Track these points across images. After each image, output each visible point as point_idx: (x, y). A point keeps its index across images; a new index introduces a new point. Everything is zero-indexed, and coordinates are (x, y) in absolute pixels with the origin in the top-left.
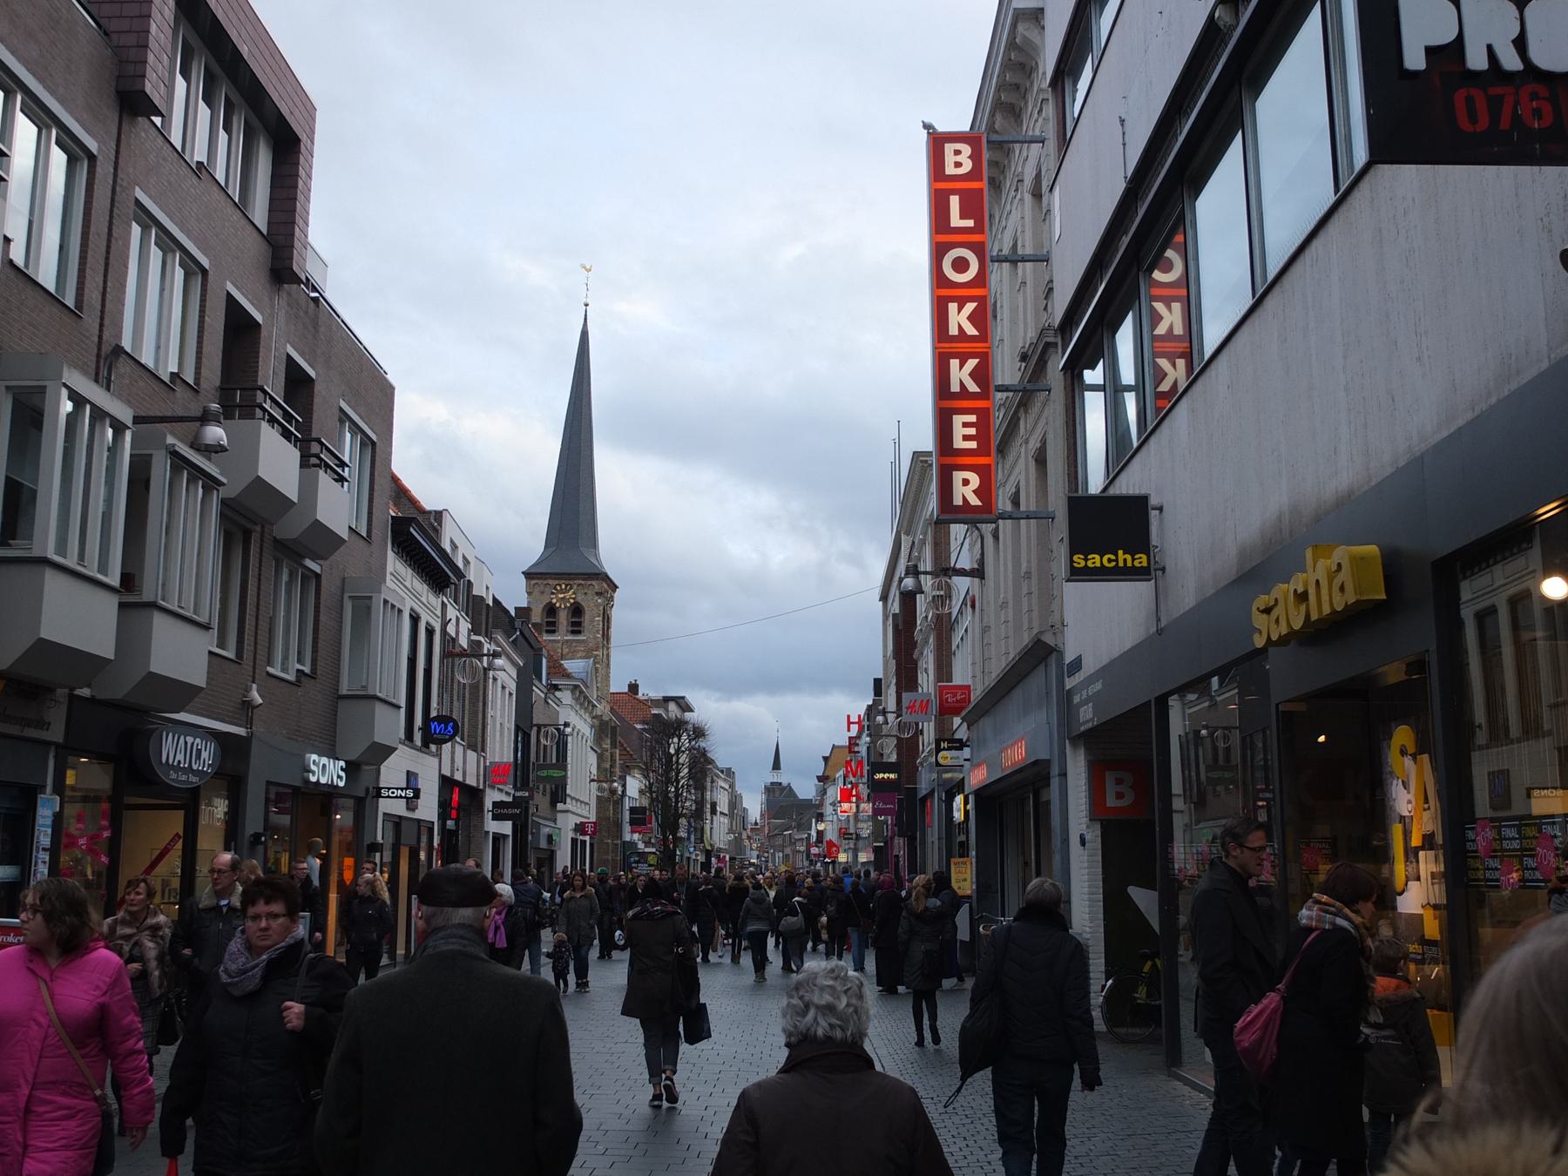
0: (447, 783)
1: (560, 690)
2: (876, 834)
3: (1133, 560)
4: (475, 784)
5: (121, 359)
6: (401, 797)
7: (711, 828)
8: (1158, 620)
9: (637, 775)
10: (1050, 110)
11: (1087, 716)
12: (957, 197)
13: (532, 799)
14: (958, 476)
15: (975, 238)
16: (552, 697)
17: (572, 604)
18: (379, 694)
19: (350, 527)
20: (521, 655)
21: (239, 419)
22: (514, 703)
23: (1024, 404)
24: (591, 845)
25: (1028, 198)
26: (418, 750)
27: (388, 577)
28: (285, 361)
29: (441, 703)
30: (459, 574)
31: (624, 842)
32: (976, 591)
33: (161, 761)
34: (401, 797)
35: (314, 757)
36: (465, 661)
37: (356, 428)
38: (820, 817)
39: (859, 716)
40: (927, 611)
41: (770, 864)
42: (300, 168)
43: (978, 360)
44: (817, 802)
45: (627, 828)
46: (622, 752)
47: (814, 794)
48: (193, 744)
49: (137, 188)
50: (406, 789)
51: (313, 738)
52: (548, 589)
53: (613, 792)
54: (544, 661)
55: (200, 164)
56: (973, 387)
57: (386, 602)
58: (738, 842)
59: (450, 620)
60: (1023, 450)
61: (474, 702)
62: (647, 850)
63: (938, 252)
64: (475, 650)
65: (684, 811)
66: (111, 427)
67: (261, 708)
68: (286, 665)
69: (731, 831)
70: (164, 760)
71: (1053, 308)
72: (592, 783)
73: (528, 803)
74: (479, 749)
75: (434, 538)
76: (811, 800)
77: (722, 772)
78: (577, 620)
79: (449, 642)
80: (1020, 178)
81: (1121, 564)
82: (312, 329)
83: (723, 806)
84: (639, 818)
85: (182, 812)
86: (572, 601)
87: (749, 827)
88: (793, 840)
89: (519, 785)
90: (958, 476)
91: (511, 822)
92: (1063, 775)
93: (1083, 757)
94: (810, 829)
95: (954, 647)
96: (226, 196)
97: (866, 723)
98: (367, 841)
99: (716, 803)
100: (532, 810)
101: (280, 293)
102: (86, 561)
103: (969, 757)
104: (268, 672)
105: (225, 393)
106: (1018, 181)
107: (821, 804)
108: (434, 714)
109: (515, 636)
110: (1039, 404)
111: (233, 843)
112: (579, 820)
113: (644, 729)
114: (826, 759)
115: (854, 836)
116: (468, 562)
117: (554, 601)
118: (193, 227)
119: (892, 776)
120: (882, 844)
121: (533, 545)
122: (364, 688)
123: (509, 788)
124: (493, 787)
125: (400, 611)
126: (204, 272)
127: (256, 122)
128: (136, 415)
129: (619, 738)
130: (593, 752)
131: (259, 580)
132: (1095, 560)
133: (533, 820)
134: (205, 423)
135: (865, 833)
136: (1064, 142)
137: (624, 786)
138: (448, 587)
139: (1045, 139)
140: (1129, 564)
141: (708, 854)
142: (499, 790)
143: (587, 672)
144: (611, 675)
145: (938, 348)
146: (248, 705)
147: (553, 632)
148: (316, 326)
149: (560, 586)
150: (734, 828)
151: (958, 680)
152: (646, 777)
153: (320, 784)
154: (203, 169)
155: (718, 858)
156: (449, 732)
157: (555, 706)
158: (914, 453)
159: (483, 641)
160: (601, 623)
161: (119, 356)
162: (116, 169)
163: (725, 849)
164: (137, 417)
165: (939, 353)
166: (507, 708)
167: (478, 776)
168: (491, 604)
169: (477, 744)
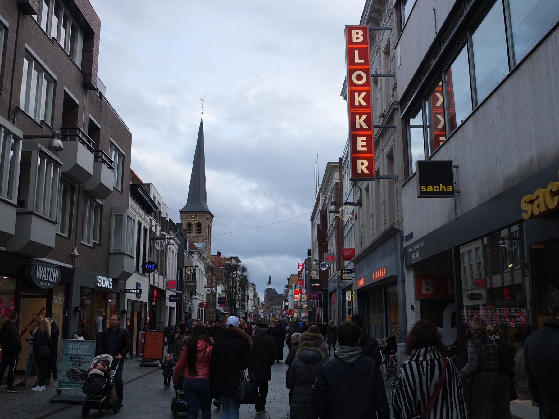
0: (152, 288)
1: (193, 254)
2: (309, 307)
3: (446, 188)
4: (162, 288)
5: (19, 112)
6: (134, 293)
7: (247, 305)
8: (456, 214)
9: (221, 285)
10: (394, 17)
11: (416, 257)
12: (358, 51)
13: (184, 294)
14: (360, 161)
15: (365, 67)
16: (190, 256)
17: (197, 223)
18: (126, 252)
19: (114, 187)
20: (179, 240)
21: (69, 141)
22: (177, 258)
23: (382, 135)
24: (205, 311)
25: (383, 55)
26: (140, 275)
27: (129, 207)
28: (88, 120)
29: (149, 257)
30: (157, 208)
31: (216, 310)
32: (357, 212)
33: (36, 278)
34: (134, 293)
35: (100, 277)
36: (159, 241)
37: (117, 149)
38: (286, 301)
39: (302, 263)
40: (333, 222)
41: (267, 318)
42: (94, 43)
43: (367, 115)
44: (284, 295)
45: (217, 305)
46: (215, 277)
47: (283, 292)
48: (50, 271)
49: (26, 44)
50: (136, 290)
51: (99, 269)
52: (188, 217)
53: (212, 291)
54: (188, 242)
55: (53, 38)
56: (365, 126)
57: (128, 216)
58: (256, 310)
59: (153, 225)
60: (381, 154)
61: (162, 257)
62: (225, 313)
63: (350, 72)
64: (163, 237)
65: (239, 298)
66: (13, 138)
67: (78, 257)
68: (88, 241)
69: (254, 306)
70: (37, 277)
71: (397, 94)
72: (205, 288)
73: (182, 295)
74: (164, 275)
75: (147, 193)
76: (282, 294)
77: (251, 284)
78: (199, 228)
79: (153, 234)
80: (379, 47)
81: (441, 190)
82: (99, 109)
83: (251, 297)
84: (222, 301)
85: (46, 299)
86: (197, 221)
87: (261, 304)
88: (276, 309)
89: (178, 289)
90: (360, 161)
91: (176, 303)
92: (403, 281)
93: (412, 274)
94: (282, 305)
95: (345, 235)
96: (64, 52)
97: (305, 266)
98: (121, 310)
99: (249, 295)
100: (183, 298)
101: (86, 93)
102: (2, 193)
103: (354, 276)
104: (81, 243)
105: (63, 129)
106: (378, 48)
107: (287, 295)
108: (147, 261)
109: (177, 233)
110: (389, 134)
111: (67, 311)
112: (200, 302)
113: (224, 269)
114: (288, 279)
115: (300, 307)
116: (160, 204)
117: (191, 221)
118: (50, 63)
119: (318, 285)
120: (312, 310)
121: (182, 200)
122: (120, 250)
123: (175, 290)
124: (169, 289)
125: (134, 220)
126: (55, 81)
127: (76, 24)
128: (24, 135)
129: (214, 272)
130: (205, 277)
131: (78, 206)
132: (430, 189)
133: (184, 302)
134: (54, 138)
135: (305, 306)
136: (401, 30)
137: (216, 289)
138: (152, 213)
139: (392, 28)
140: (445, 190)
141: (246, 314)
142: (172, 291)
143: (203, 247)
144: (211, 249)
145: (351, 110)
146: (73, 256)
147: (190, 233)
148: (101, 108)
149: (193, 216)
150: (255, 305)
151: (347, 245)
152: (224, 286)
153: (103, 287)
154: (55, 40)
155: (250, 315)
156: (153, 268)
157: (191, 259)
158: (328, 162)
159: (165, 234)
160: (208, 230)
161: (18, 111)
162: (17, 34)
163: (252, 312)
164: (25, 136)
165: (351, 112)
166: (174, 260)
167: (164, 285)
168: (168, 220)
169: (163, 273)
